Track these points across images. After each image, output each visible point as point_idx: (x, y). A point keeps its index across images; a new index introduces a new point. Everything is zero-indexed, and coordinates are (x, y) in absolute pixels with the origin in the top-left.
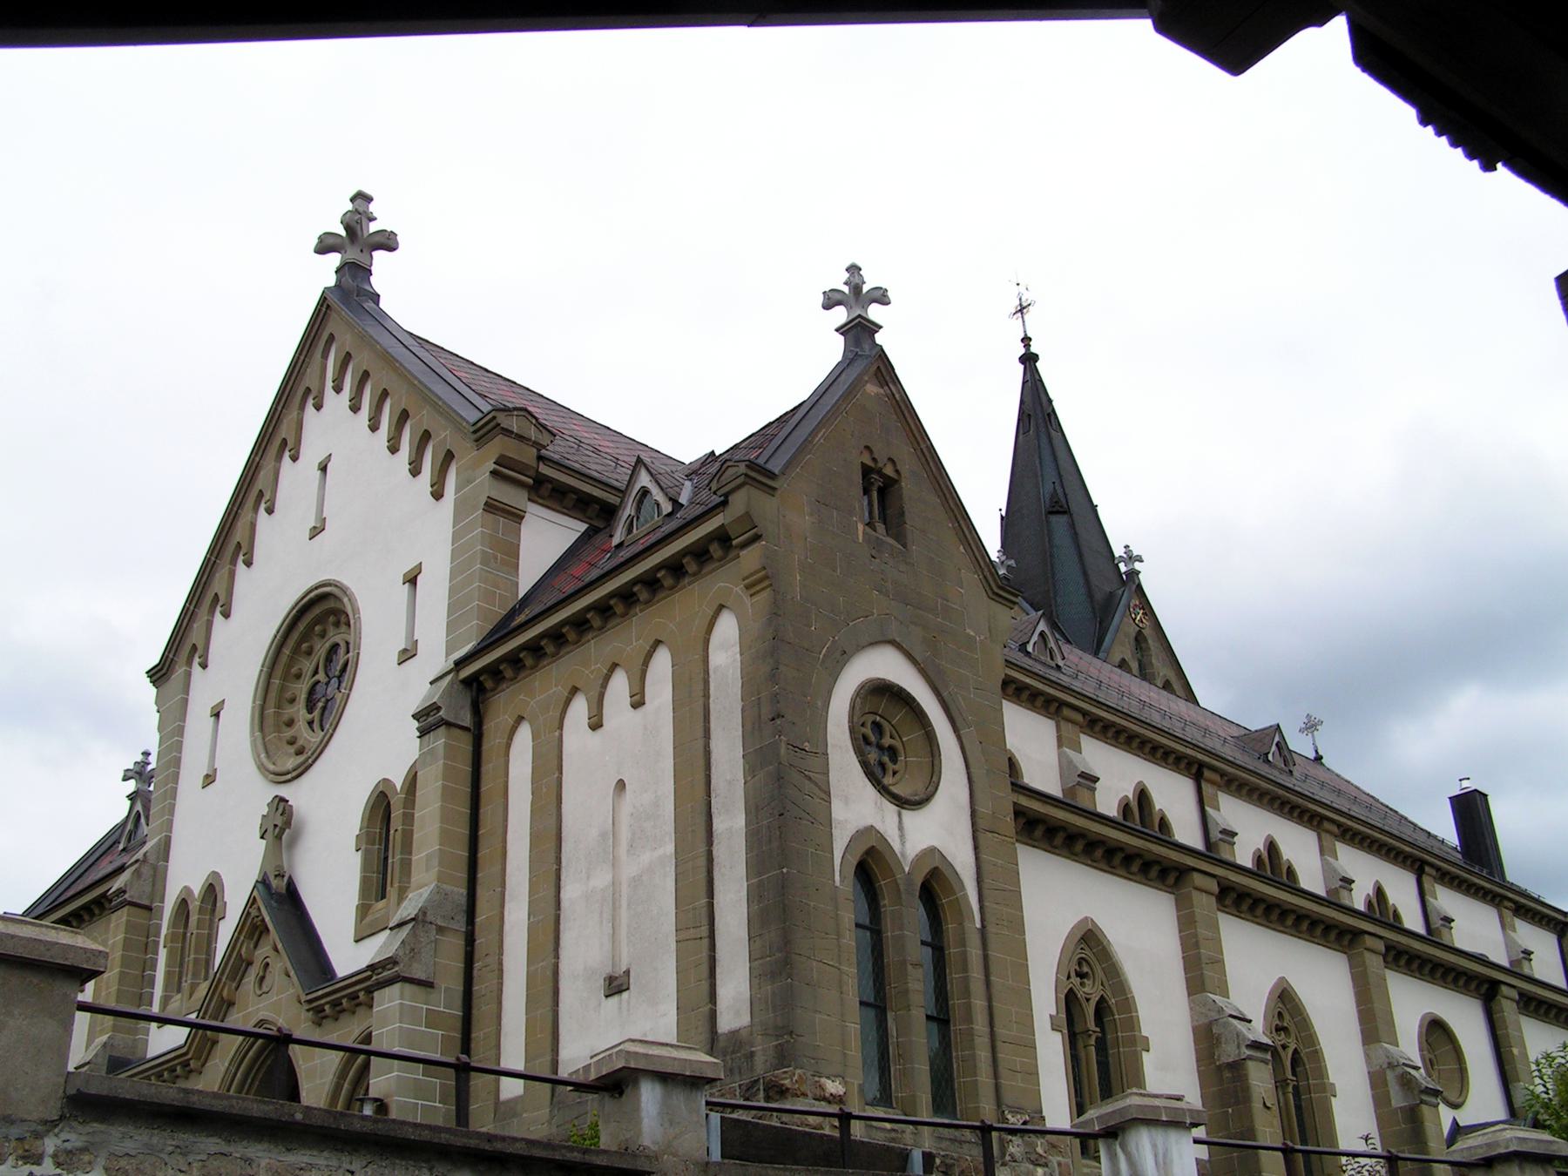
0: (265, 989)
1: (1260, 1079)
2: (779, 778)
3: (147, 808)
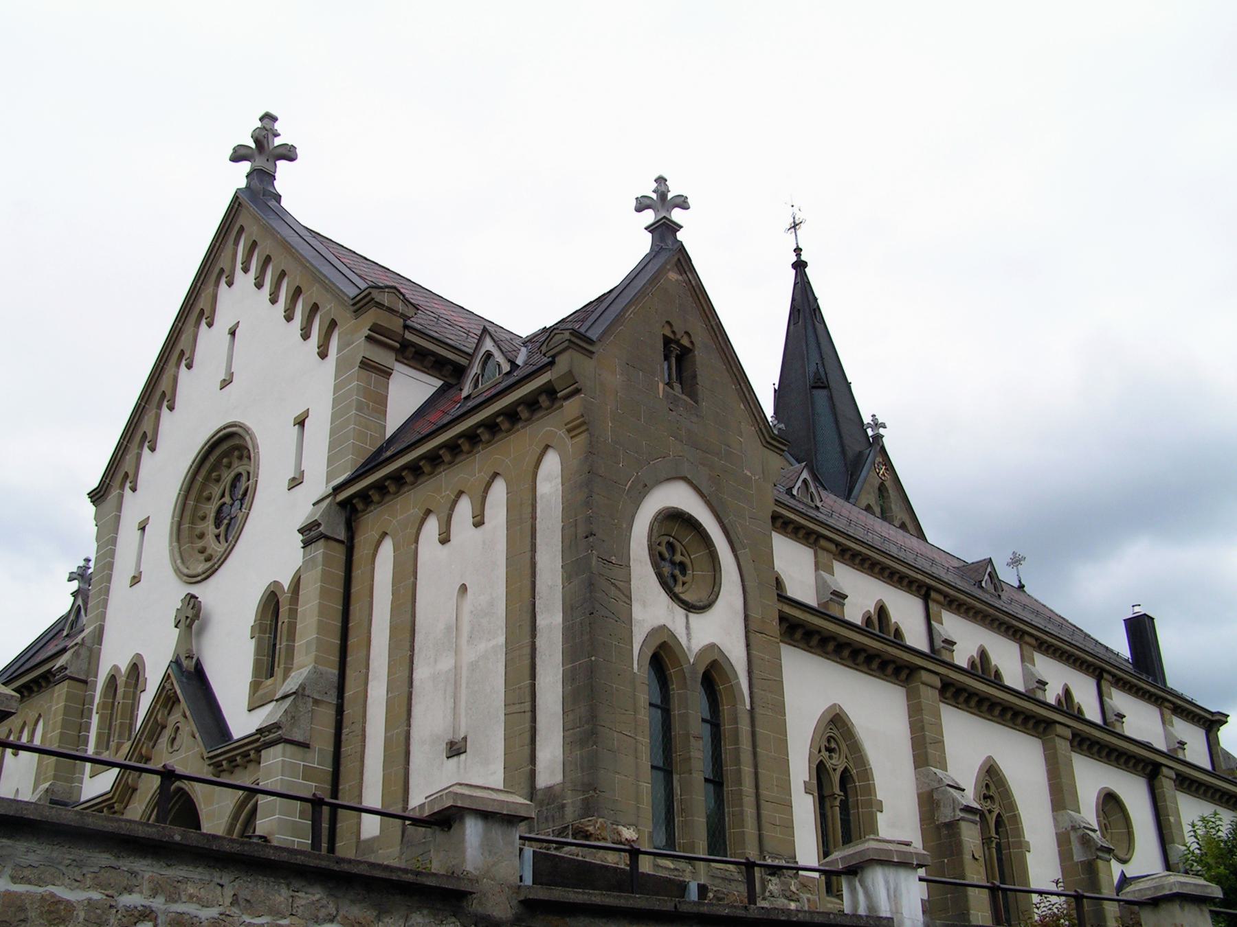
0: (175, 747)
1: (970, 836)
2: (591, 585)
3: (86, 603)
